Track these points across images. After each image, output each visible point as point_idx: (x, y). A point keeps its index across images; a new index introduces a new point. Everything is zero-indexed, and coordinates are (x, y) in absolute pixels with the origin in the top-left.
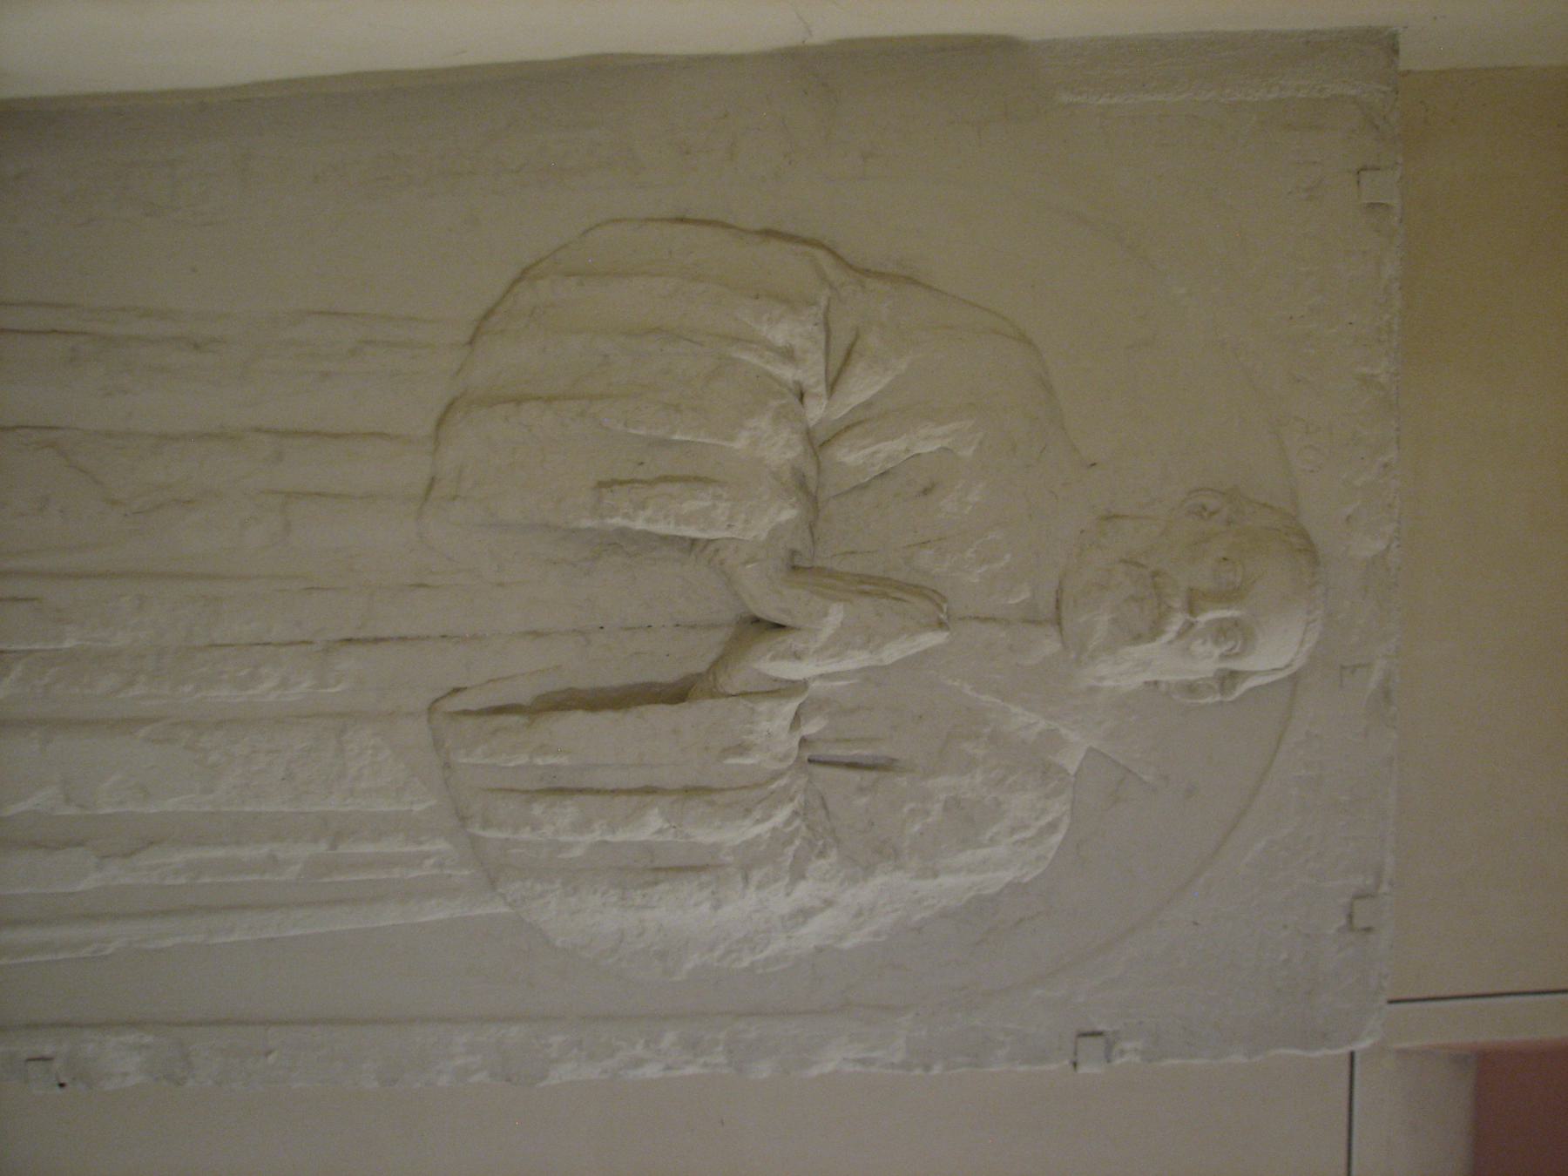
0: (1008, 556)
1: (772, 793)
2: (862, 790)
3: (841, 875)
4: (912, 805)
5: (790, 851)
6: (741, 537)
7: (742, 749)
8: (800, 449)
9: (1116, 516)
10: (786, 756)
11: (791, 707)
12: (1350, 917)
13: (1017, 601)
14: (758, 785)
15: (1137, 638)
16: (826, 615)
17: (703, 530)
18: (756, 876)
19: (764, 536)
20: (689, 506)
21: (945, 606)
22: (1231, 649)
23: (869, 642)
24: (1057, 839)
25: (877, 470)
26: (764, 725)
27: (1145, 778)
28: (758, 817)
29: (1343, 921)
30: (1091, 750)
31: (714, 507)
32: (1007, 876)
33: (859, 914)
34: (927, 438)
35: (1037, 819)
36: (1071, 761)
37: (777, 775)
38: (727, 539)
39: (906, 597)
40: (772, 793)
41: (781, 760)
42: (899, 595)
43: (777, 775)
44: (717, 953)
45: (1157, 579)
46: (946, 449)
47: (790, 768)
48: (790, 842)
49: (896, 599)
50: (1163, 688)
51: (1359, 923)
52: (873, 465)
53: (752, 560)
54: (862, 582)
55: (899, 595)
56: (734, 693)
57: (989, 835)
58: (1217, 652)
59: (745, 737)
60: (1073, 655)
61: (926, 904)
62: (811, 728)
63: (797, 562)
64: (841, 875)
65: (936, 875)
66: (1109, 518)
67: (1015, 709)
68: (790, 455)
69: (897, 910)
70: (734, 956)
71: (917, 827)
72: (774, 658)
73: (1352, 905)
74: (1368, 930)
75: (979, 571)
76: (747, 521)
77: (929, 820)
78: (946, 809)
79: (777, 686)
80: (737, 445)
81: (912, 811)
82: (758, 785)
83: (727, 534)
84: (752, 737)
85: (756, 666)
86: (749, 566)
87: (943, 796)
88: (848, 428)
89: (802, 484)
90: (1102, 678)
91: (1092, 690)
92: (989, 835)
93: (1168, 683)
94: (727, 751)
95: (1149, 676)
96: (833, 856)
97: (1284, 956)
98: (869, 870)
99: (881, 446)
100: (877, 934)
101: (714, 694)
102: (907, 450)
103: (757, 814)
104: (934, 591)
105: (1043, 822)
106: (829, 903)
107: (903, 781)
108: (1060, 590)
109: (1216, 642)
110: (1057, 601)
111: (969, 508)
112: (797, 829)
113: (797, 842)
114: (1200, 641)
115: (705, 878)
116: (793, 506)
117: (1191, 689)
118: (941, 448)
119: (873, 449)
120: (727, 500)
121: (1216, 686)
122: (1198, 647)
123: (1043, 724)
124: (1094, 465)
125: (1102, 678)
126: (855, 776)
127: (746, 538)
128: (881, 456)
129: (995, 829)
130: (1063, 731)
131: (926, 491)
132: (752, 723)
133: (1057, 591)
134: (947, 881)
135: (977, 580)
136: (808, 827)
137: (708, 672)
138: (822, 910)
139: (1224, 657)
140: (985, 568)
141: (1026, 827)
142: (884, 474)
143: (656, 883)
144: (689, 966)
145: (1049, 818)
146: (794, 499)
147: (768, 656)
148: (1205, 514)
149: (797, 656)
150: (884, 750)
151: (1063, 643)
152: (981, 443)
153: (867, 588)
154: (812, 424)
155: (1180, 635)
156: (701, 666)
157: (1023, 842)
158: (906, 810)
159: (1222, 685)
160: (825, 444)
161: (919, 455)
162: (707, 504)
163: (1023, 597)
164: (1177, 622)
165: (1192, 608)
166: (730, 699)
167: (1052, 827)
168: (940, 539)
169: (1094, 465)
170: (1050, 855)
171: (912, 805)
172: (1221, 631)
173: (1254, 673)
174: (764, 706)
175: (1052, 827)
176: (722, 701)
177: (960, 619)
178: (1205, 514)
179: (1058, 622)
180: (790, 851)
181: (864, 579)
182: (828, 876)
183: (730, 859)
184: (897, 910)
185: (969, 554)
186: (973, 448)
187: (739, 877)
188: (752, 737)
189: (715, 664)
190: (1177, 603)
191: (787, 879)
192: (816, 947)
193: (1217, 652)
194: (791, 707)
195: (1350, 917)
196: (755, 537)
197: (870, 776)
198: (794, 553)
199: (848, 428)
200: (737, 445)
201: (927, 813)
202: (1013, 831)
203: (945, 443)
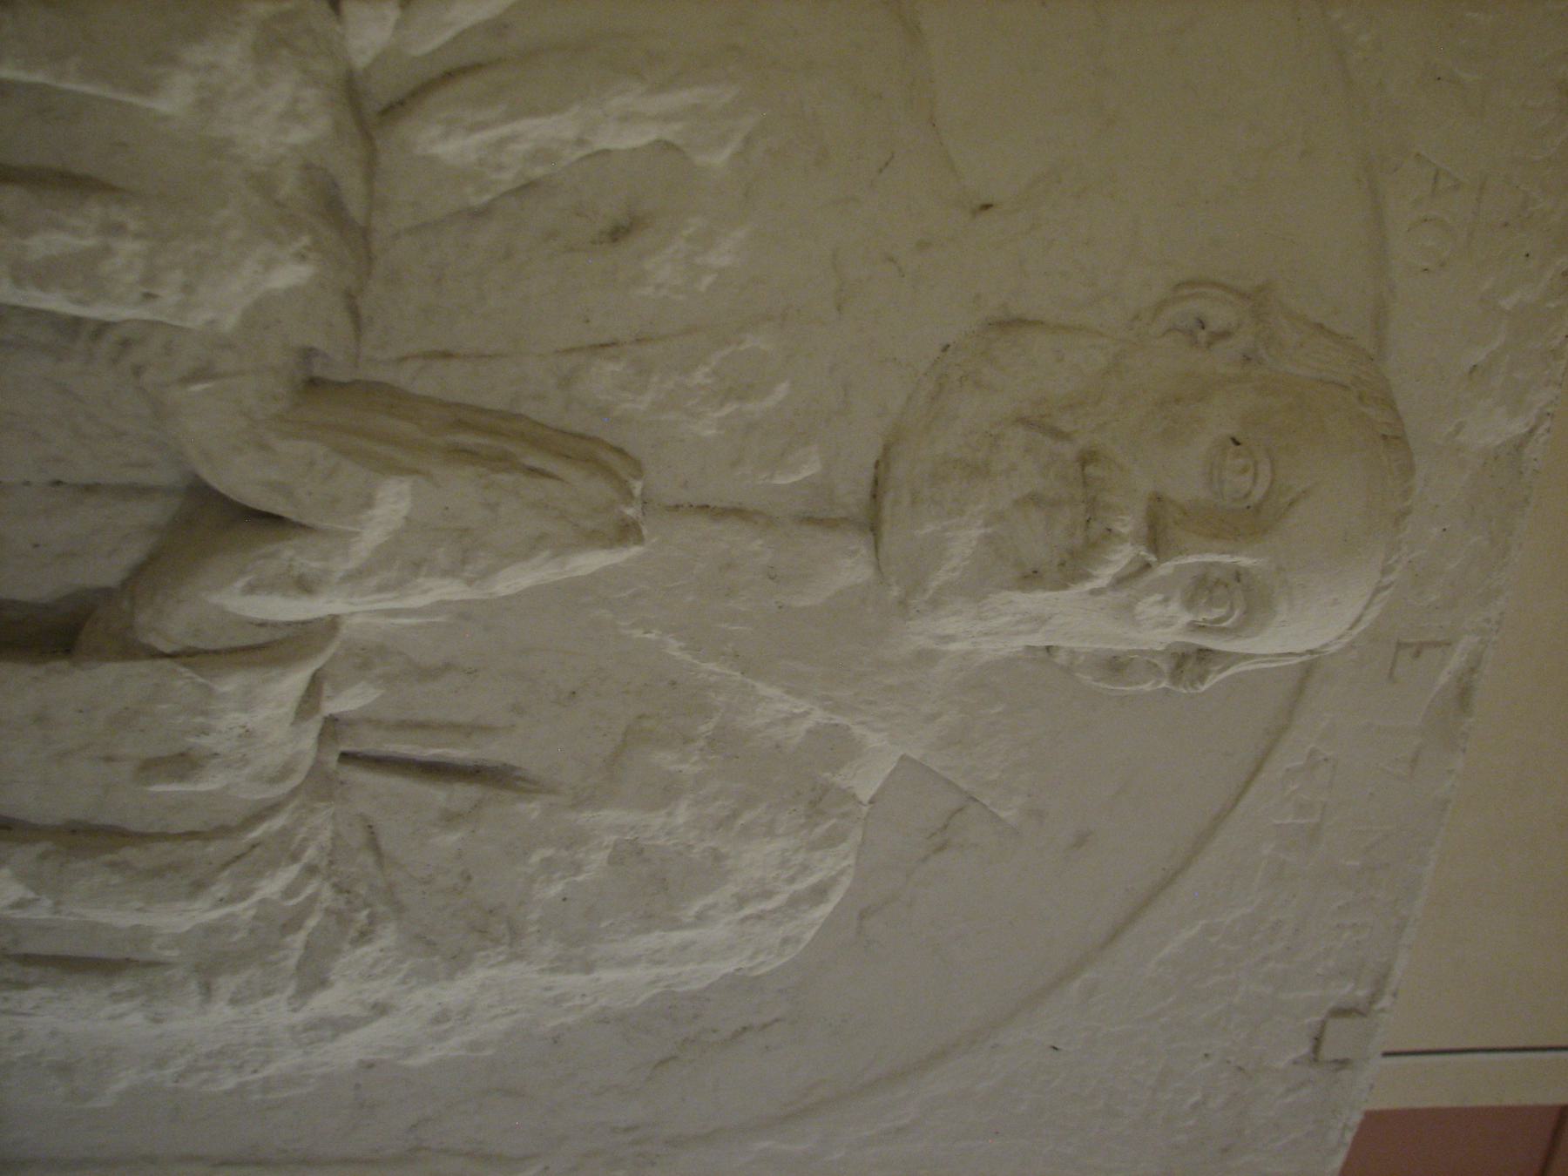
0: (782, 390)
1: (254, 846)
2: (450, 819)
3: (406, 966)
4: (549, 852)
5: (298, 940)
6: (177, 323)
7: (184, 763)
8: (322, 125)
9: (1021, 322)
10: (285, 772)
11: (296, 680)
12: (1317, 1041)
13: (793, 479)
14: (223, 831)
15: (1031, 578)
16: (369, 503)
17: (80, 302)
18: (227, 984)
19: (230, 322)
20: (43, 245)
21: (637, 487)
22: (1219, 620)
23: (464, 562)
24: (823, 911)
25: (507, 179)
26: (233, 719)
27: (1003, 814)
28: (220, 895)
29: (1305, 1049)
30: (903, 758)
31: (107, 251)
32: (728, 967)
33: (437, 1020)
34: (627, 118)
35: (792, 880)
36: (866, 782)
37: (272, 809)
38: (455, 39)
39: (551, 465)
40: (254, 846)
41: (273, 781)
42: (535, 460)
43: (272, 809)
44: (169, 1072)
45: (1090, 469)
46: (665, 146)
47: (294, 793)
48: (293, 924)
49: (533, 471)
50: (1061, 658)
51: (1328, 1052)
52: (500, 168)
53: (201, 373)
54: (460, 425)
55: (535, 460)
56: (168, 649)
57: (696, 907)
58: (1186, 617)
59: (192, 740)
60: (895, 592)
61: (566, 1005)
62: (346, 701)
63: (318, 370)
64: (406, 966)
65: (588, 968)
66: (1009, 324)
67: (763, 689)
68: (299, 135)
69: (513, 1012)
70: (205, 1075)
71: (556, 889)
72: (251, 589)
73: (1323, 1024)
74: (1343, 1063)
75: (717, 415)
76: (188, 288)
77: (580, 878)
78: (616, 860)
79: (263, 636)
80: (162, 105)
81: (548, 863)
82: (223, 831)
83: (144, 313)
84: (206, 741)
85: (215, 599)
86: (198, 388)
87: (611, 839)
88: (449, 76)
89: (331, 206)
90: (951, 638)
91: (926, 657)
92: (696, 907)
93: (1072, 652)
94: (151, 768)
95: (1039, 640)
96: (388, 936)
97: (1196, 1097)
98: (459, 962)
99: (522, 125)
100: (475, 1046)
101: (132, 650)
102: (580, 142)
103: (221, 889)
104: (620, 451)
105: (802, 885)
106: (381, 1009)
107: (532, 809)
108: (882, 465)
109: (1190, 603)
110: (876, 482)
111: (708, 280)
112: (313, 899)
113: (312, 923)
114: (1159, 597)
115: (122, 985)
116: (301, 258)
117: (1115, 666)
118: (658, 141)
119: (505, 130)
120: (138, 236)
121: (1165, 667)
122: (1149, 607)
123: (819, 716)
124: (987, 207)
125: (951, 638)
126: (439, 795)
127: (188, 325)
128: (522, 147)
129: (710, 899)
130: (857, 731)
131: (617, 234)
132: (204, 713)
133: (877, 465)
134: (607, 975)
135: (710, 433)
136: (339, 888)
137: (124, 584)
138: (366, 1021)
139: (1195, 627)
140: (728, 409)
141: (767, 895)
142: (527, 188)
143: (23, 985)
144: (122, 1085)
145: (813, 879)
146: (306, 240)
147: (241, 583)
148: (1202, 335)
149: (305, 586)
150: (492, 752)
151: (878, 568)
152: (748, 140)
153: (468, 439)
154: (361, 61)
155: (1120, 581)
156: (106, 571)
157: (760, 917)
158: (535, 858)
159: (1179, 666)
160: (395, 109)
161: (606, 152)
162: (91, 242)
163: (806, 472)
164: (1122, 557)
165: (1156, 538)
166: (160, 662)
167: (819, 893)
168: (638, 341)
169: (987, 207)
170: (809, 936)
171: (549, 852)
172: (1203, 587)
173: (1247, 657)
174: (231, 684)
175: (819, 893)
176: (143, 667)
177: (668, 508)
178: (1202, 335)
179: (872, 526)
180: (298, 940)
181: (463, 417)
182: (378, 970)
183: (171, 954)
184: (513, 1012)
185: (699, 377)
186: (727, 152)
187: (193, 985)
188: (206, 741)
189: (138, 571)
190: (1128, 524)
191: (291, 990)
192: (361, 1062)
193: (1186, 617)
194: (296, 680)
195: (1317, 1041)
196: (212, 322)
197: (462, 794)
198: (308, 354)
199: (449, 76)
200: (162, 105)
201: (578, 867)
202: (742, 901)
203: (671, 132)
